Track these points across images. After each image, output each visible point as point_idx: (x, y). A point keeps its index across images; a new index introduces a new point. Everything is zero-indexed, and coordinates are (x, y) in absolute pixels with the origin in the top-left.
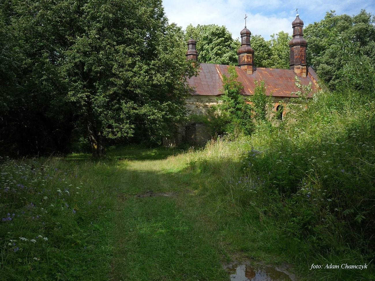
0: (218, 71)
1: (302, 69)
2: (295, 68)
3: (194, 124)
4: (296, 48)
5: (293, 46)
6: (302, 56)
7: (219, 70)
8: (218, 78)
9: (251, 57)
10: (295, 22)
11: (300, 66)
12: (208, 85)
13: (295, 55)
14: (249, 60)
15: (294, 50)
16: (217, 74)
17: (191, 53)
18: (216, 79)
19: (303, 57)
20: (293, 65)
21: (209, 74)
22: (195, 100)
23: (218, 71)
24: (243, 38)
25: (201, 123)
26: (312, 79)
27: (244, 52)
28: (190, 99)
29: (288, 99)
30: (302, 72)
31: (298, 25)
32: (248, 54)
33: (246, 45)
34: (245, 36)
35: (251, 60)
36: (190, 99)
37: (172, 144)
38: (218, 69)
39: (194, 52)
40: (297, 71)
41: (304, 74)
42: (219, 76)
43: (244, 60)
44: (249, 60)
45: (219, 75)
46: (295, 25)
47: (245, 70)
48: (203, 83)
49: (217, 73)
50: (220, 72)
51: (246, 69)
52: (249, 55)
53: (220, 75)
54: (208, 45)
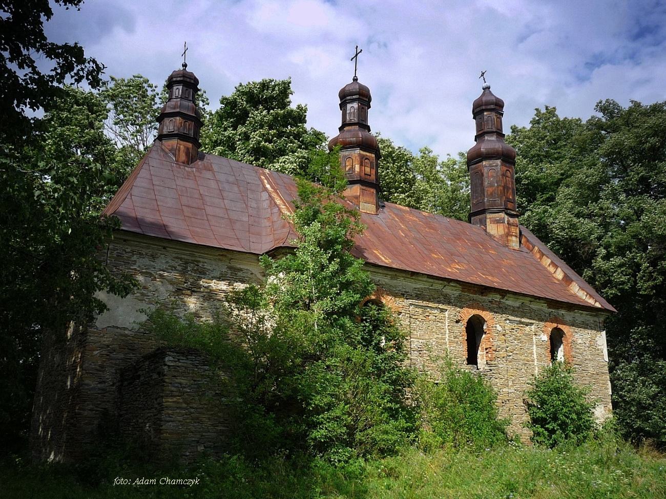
0: (268, 186)
1: (508, 224)
2: (488, 220)
3: (158, 355)
4: (491, 166)
5: (481, 161)
6: (505, 187)
7: (269, 183)
8: (266, 204)
9: (372, 163)
10: (484, 99)
11: (502, 215)
12: (232, 222)
13: (486, 183)
14: (368, 170)
15: (485, 170)
16: (265, 196)
17: (178, 110)
18: (258, 208)
19: (510, 191)
20: (483, 212)
21: (236, 189)
22: (173, 263)
23: (268, 186)
24: (349, 106)
25: (187, 352)
26: (538, 256)
27: (350, 143)
28: (153, 257)
29: (497, 297)
30: (508, 234)
31: (492, 106)
32: (365, 151)
33: (357, 127)
34: (353, 101)
35: (374, 172)
36: (153, 257)
37: (48, 449)
38: (267, 178)
39: (188, 108)
40: (495, 230)
41: (514, 238)
42: (273, 204)
43: (352, 168)
44: (368, 170)
45: (270, 196)
46: (484, 107)
47: (355, 201)
48: (209, 210)
49: (266, 189)
50: (272, 187)
51: (357, 198)
52: (368, 154)
53: (274, 195)
54: (235, 128)
